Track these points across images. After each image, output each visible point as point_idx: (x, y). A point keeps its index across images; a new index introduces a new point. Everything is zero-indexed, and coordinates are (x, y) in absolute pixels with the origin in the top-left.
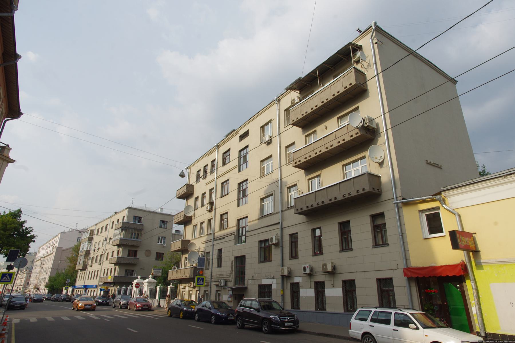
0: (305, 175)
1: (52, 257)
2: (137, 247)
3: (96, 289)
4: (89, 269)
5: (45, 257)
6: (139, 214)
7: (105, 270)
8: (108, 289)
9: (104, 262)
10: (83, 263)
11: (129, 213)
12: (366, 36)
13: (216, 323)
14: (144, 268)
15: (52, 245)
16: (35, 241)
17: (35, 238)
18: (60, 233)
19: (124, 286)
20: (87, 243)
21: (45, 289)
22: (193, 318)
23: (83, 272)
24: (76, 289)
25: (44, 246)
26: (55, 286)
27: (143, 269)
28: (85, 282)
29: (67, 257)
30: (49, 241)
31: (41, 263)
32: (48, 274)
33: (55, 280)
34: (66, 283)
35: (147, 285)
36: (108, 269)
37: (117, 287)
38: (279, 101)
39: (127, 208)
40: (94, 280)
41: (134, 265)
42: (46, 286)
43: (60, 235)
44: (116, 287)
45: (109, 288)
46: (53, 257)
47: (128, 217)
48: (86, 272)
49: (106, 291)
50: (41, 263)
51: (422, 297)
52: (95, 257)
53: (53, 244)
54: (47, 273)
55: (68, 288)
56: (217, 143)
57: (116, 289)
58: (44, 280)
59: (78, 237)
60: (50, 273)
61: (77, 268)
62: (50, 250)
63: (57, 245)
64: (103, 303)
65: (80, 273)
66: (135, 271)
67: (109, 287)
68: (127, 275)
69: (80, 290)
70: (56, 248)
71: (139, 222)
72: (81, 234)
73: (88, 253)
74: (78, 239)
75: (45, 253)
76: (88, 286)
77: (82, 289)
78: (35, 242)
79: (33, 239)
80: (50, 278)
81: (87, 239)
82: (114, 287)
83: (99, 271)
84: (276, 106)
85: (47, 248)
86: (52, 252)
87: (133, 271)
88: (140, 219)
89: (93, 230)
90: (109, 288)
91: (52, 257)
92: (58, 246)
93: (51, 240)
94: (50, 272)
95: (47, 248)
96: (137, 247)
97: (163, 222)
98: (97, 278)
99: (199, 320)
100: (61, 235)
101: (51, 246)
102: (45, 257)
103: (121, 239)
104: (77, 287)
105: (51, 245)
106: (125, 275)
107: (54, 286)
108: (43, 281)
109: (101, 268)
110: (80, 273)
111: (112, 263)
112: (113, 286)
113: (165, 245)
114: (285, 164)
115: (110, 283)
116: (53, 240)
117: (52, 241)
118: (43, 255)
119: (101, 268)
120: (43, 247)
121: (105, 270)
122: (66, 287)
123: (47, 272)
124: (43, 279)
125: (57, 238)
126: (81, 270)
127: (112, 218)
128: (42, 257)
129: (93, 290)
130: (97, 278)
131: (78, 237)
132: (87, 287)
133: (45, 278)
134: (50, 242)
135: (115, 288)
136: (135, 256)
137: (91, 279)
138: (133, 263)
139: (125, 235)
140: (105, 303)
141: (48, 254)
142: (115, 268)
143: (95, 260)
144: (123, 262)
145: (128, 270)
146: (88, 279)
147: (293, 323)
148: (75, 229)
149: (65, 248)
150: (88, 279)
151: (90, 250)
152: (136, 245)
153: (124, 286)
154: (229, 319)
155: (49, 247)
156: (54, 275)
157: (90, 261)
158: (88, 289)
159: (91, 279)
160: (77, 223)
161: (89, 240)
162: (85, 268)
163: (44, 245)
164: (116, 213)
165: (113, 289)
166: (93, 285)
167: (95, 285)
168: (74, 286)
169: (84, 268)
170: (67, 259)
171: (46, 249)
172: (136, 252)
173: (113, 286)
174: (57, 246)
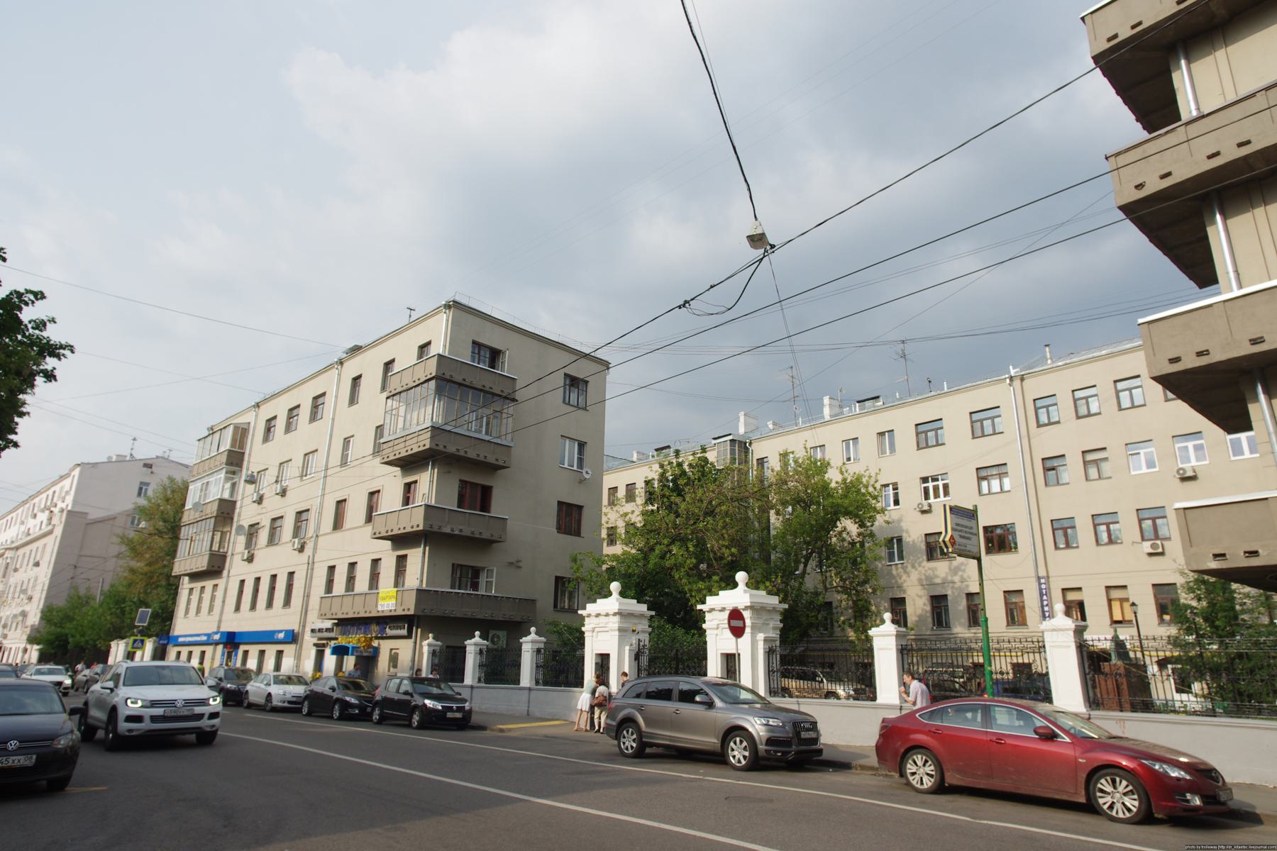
0: (402, 475)
1: (49, 549)
2: (493, 468)
3: (289, 650)
4: (237, 569)
5: (17, 548)
6: (492, 338)
7: (332, 569)
8: (370, 646)
9: (320, 539)
10: (211, 550)
11: (456, 325)
12: (389, 332)
13: (422, 726)
14: (518, 561)
15: (46, 508)
16: (56, 373)
17: (58, 357)
18: (79, 465)
19: (477, 633)
20: (222, 475)
21: (25, 650)
22: (299, 711)
23: (209, 584)
24: (178, 649)
25: (14, 515)
26: (73, 636)
27: (515, 565)
28: (220, 621)
29: (118, 536)
30: (32, 497)
31: (7, 568)
32: (35, 600)
33: (69, 618)
34: (136, 624)
35: (616, 626)
36: (274, 577)
37: (424, 637)
38: (342, 363)
39: (448, 306)
40: (271, 612)
41: (484, 544)
42: (32, 640)
43: (77, 472)
44: (421, 641)
45: (375, 643)
46: (50, 546)
47: (454, 341)
48: (221, 582)
49: (365, 654)
50: (7, 568)
51: (779, 754)
52: (266, 523)
53: (49, 503)
54: (30, 598)
55: (142, 641)
56: (446, 300)
57: (421, 647)
58: (20, 618)
59: (141, 483)
60: (44, 596)
61: (177, 570)
62: (35, 525)
63: (69, 502)
64: (450, 715)
65: (191, 590)
66: (490, 572)
67: (377, 638)
68: (459, 589)
69: (197, 651)
70: (65, 512)
71: (493, 364)
72: (152, 473)
73: (226, 511)
74: (141, 489)
75: (18, 535)
76: (242, 634)
77: (209, 650)
78: (54, 378)
79: (50, 363)
80: (48, 614)
81: (224, 458)
82: (409, 636)
83: (278, 579)
84: (334, 372)
85: (26, 517)
86: (45, 529)
87: (476, 572)
88: (495, 355)
89: (245, 427)
90: (375, 643)
91: (49, 549)
92: (73, 507)
93: (39, 493)
94: (45, 593)
95: (26, 517)
96: (493, 468)
97: (574, 382)
98: (287, 602)
99: (309, 714)
100: (81, 473)
101: (43, 511)
102: (17, 548)
103: (435, 430)
104: (181, 640)
105: (42, 506)
106: (451, 588)
107: (71, 640)
108: (14, 625)
109: (311, 565)
110: (191, 590)
111: (384, 534)
112: (404, 632)
113: (587, 473)
114: (372, 452)
115: (384, 621)
116: (50, 492)
117: (44, 496)
118: (12, 542)
119: (311, 565)
120: (9, 518)
121: (332, 569)
122: (135, 641)
123: (29, 593)
124: (15, 616)
125: (67, 483)
126: (195, 576)
127: (345, 365)
128: (6, 549)
129: (271, 651)
130: (287, 602)
131: (141, 483)
132: (237, 641)
133: (24, 614)
134: (36, 500)
135: (415, 643)
136: (485, 506)
137: (270, 604)
138: (484, 536)
139: (447, 412)
140: (458, 715)
141: (29, 538)
142: (402, 560)
143: (263, 536)
144: (447, 530)
145: (462, 566)
146: (238, 609)
147: (448, 716)
148: (129, 456)
149: (94, 514)
150: (238, 609)
151: (234, 503)
152: (491, 459)
153: (477, 633)
154: (448, 716)
155: (35, 516)
156: (61, 602)
157: (242, 540)
158: (242, 648)
159: (270, 604)
160: (134, 439)
161: (229, 463)
162: (216, 569)
163: (11, 512)
164: (356, 350)
165: (405, 648)
166: (273, 632)
167: (287, 632)
168: (168, 638)
169: (215, 568)
170: (122, 543)
171: (22, 523)
172: (486, 492)
173: (404, 632)
174: (69, 508)
